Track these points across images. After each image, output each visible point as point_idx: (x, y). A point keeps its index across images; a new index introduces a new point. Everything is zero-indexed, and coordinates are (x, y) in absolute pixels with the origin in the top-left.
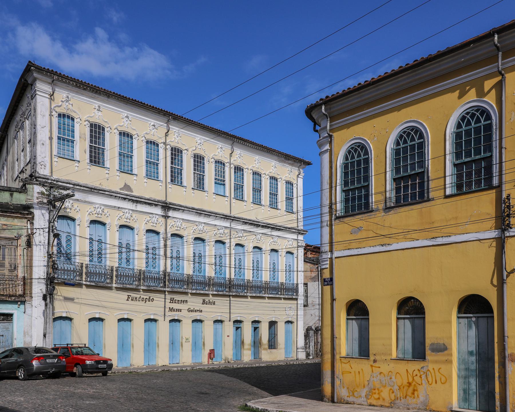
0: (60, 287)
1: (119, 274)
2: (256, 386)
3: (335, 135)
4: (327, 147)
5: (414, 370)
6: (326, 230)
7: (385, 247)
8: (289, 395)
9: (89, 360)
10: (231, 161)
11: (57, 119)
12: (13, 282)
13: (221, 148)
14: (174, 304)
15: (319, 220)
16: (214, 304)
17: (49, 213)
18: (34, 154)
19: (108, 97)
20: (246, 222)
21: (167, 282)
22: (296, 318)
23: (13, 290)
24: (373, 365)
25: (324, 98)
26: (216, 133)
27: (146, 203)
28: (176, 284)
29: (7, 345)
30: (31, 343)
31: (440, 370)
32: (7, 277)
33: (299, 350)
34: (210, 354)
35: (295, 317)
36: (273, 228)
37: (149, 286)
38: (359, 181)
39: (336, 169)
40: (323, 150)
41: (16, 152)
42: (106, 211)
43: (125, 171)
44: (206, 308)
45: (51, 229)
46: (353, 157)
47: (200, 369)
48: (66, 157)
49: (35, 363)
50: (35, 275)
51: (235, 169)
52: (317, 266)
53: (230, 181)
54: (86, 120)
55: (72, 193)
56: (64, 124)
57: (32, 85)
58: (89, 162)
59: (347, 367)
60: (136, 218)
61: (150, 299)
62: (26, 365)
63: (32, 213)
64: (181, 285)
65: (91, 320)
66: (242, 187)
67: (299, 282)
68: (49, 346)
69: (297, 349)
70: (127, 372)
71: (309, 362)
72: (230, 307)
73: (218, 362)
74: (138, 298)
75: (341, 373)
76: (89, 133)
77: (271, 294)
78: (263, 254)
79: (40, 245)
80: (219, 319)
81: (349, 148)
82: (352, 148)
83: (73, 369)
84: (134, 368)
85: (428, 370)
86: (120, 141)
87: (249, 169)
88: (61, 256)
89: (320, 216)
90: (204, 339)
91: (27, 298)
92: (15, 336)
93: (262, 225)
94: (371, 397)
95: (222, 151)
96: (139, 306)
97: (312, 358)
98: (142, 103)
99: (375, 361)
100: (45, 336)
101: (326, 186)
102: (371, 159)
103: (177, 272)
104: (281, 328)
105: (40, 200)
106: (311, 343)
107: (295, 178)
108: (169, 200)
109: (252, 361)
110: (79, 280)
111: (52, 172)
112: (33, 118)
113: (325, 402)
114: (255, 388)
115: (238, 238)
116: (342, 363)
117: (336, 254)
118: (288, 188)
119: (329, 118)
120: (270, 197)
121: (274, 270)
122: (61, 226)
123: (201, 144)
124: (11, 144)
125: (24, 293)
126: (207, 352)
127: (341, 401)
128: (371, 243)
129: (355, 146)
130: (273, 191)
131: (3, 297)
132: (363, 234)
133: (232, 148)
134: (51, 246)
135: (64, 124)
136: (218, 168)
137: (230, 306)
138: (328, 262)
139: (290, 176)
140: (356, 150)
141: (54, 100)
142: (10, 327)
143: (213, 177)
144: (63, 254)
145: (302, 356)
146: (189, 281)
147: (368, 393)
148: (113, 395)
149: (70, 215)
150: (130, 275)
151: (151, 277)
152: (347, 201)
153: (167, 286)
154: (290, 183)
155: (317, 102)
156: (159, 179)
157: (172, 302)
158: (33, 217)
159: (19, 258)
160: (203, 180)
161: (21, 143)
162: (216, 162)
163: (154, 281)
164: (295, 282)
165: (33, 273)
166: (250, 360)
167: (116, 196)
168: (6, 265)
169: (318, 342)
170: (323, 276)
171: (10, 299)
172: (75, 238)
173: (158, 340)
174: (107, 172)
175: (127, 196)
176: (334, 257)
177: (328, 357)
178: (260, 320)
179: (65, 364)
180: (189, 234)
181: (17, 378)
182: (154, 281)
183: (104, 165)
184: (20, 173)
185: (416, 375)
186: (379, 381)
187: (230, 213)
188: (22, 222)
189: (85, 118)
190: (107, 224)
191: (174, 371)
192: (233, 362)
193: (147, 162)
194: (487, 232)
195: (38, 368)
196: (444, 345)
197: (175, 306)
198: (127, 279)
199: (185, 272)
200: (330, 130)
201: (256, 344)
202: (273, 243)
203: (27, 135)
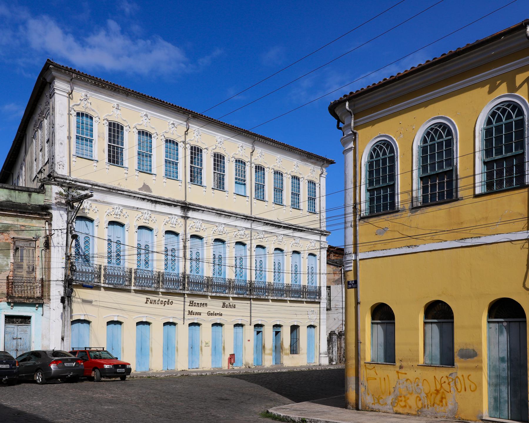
0: (78, 289)
1: (138, 276)
4: (352, 145)
5: (443, 377)
6: (350, 231)
8: (312, 402)
9: (107, 364)
10: (252, 160)
11: (75, 118)
12: (31, 284)
13: (242, 147)
14: (193, 307)
16: (234, 307)
17: (68, 214)
18: (52, 153)
19: (127, 95)
20: (268, 223)
21: (186, 285)
22: (319, 322)
24: (400, 371)
25: (348, 94)
27: (165, 204)
29: (25, 348)
31: (470, 377)
33: (321, 355)
34: (230, 358)
36: (295, 229)
37: (169, 289)
38: (384, 180)
39: (361, 168)
40: (347, 148)
41: (35, 152)
42: (124, 211)
44: (225, 311)
45: (69, 230)
48: (85, 157)
49: (52, 366)
50: (53, 278)
51: (256, 168)
54: (105, 119)
55: (91, 194)
56: (83, 123)
57: (50, 84)
58: (107, 162)
59: (371, 373)
60: (155, 219)
61: (169, 302)
62: (44, 369)
63: (50, 214)
64: (200, 287)
65: (109, 323)
66: (263, 187)
67: (322, 285)
68: (67, 348)
69: (320, 354)
70: (145, 377)
75: (365, 379)
76: (108, 132)
77: (293, 297)
79: (58, 247)
80: (240, 323)
81: (374, 146)
82: (377, 146)
83: (91, 373)
84: (154, 373)
85: (457, 377)
87: (271, 169)
88: (79, 258)
90: (224, 343)
92: (33, 339)
93: (284, 226)
94: (398, 404)
98: (161, 101)
99: (401, 367)
100: (63, 339)
101: (350, 185)
102: (397, 158)
104: (303, 332)
105: (58, 200)
106: (334, 348)
108: (189, 201)
110: (97, 282)
111: (70, 172)
113: (349, 409)
114: (277, 395)
121: (296, 272)
122: (79, 226)
123: (221, 143)
125: (42, 296)
126: (227, 356)
129: (380, 144)
130: (295, 191)
131: (21, 300)
132: (388, 236)
133: (253, 146)
134: (69, 247)
135: (83, 123)
136: (239, 167)
137: (251, 309)
138: (352, 264)
139: (312, 175)
140: (381, 148)
141: (72, 99)
144: (81, 255)
146: (209, 284)
147: (393, 400)
149: (89, 216)
150: (149, 277)
152: (371, 200)
153: (186, 289)
156: (178, 179)
157: (191, 305)
158: (52, 218)
161: (40, 143)
162: (236, 161)
164: (318, 285)
166: (272, 366)
167: (134, 197)
168: (24, 267)
169: (341, 347)
171: (28, 302)
173: (177, 344)
175: (146, 196)
176: (358, 259)
177: (352, 362)
178: (281, 324)
180: (209, 235)
181: (35, 382)
182: (173, 283)
183: (123, 165)
184: (38, 173)
185: (445, 382)
187: (251, 214)
188: (40, 223)
189: (103, 117)
190: (125, 225)
191: (193, 376)
192: (253, 367)
193: (166, 161)
194: (519, 233)
195: (55, 372)
196: (474, 350)
197: (195, 309)
198: (146, 281)
201: (278, 348)
202: (295, 245)
203: (46, 135)
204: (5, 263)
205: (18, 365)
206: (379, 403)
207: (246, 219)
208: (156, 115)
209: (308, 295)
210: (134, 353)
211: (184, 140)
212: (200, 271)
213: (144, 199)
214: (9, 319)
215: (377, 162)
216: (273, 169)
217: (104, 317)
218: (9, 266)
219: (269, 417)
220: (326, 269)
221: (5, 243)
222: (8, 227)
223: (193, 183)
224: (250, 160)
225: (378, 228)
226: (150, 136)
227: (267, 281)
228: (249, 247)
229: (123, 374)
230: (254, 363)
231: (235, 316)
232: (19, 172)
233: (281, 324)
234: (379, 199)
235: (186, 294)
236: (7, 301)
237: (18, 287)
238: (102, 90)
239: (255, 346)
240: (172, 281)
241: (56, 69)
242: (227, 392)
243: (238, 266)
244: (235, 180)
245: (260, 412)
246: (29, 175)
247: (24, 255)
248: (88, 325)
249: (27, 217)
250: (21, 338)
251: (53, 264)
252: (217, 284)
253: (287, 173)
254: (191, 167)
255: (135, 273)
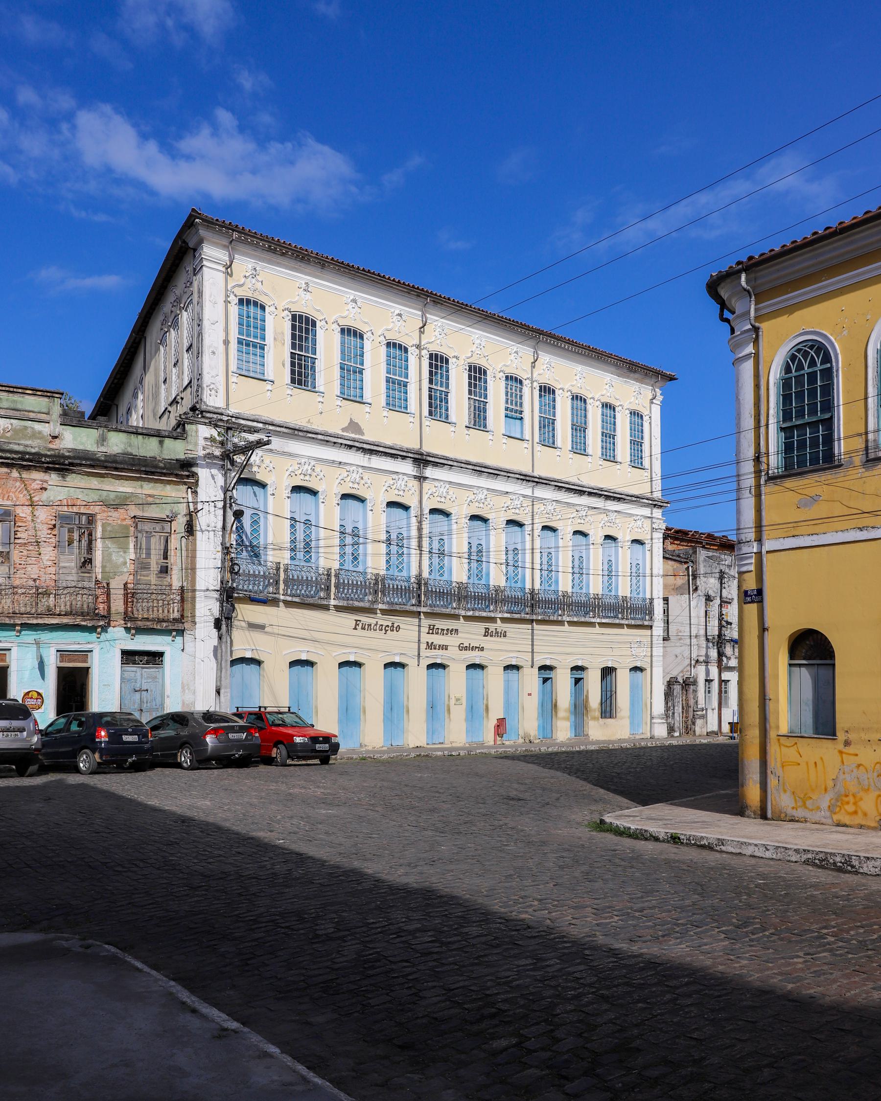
0: (240, 605)
1: (342, 581)
2: (602, 787)
3: (764, 326)
4: (750, 349)
6: (748, 504)
7: (866, 531)
8: (671, 804)
9: (299, 736)
10: (534, 376)
11: (237, 307)
12: (164, 596)
13: (516, 352)
14: (435, 636)
15: (734, 486)
16: (505, 636)
17: (225, 475)
18: (198, 370)
19: (323, 266)
20: (561, 486)
21: (423, 596)
22: (649, 661)
23: (163, 611)
24: (844, 750)
25: (745, 260)
26: (508, 325)
27: (386, 454)
28: (439, 600)
29: (154, 707)
30: (193, 703)
32: (154, 587)
33: (654, 721)
34: (498, 726)
35: (649, 660)
36: (608, 498)
37: (392, 603)
38: (813, 411)
39: (768, 389)
40: (741, 355)
41: (163, 368)
42: (318, 469)
43: (349, 398)
44: (489, 643)
45: (228, 502)
46: (800, 367)
47: (483, 753)
48: (252, 374)
49: (209, 739)
50: (200, 585)
51: (540, 390)
52: (686, 566)
53: (532, 411)
54: (285, 309)
56: (248, 317)
57: (195, 250)
59: (791, 753)
60: (369, 482)
61: (393, 626)
62: (194, 743)
63: (194, 475)
64: (447, 601)
65: (293, 664)
66: (553, 423)
67: (654, 596)
68: (226, 707)
69: (652, 718)
70: (356, 759)
71: (674, 742)
72: (532, 641)
73: (512, 742)
74: (373, 625)
75: (779, 765)
76: (290, 331)
77: (604, 617)
78: (620, 549)
79: (209, 531)
80: (514, 663)
81: (793, 351)
82: (799, 351)
83: (271, 751)
84: (367, 751)
86: (343, 344)
87: (565, 390)
88: (242, 550)
89: (735, 479)
90: (487, 700)
91: (186, 625)
92: (168, 692)
94: (841, 809)
95: (518, 358)
96: (375, 639)
97: (678, 734)
98: (380, 276)
99: (847, 743)
100: (218, 692)
101: (748, 422)
102: (837, 371)
103: (439, 578)
104: (623, 679)
105: (208, 451)
106: (676, 708)
107: (647, 404)
108: (426, 449)
109: (571, 739)
110: (273, 593)
111: (228, 405)
112: (197, 308)
113: (748, 817)
114: (602, 791)
115: (513, 511)
116: (782, 747)
117: (768, 546)
118: (635, 424)
119: (753, 298)
120: (602, 441)
121: (610, 573)
122: (243, 495)
123: (481, 347)
124: (153, 354)
125: (182, 616)
126: (493, 722)
127: (780, 816)
128: (839, 526)
129: (805, 346)
130: (607, 429)
131: (148, 623)
132: (820, 510)
133: (535, 352)
134: (229, 532)
135: (248, 317)
136: (511, 389)
137: (532, 639)
138: (753, 561)
139: (637, 402)
140: (806, 354)
141: (231, 275)
142: (159, 676)
143: (503, 406)
144: (246, 546)
145: (661, 731)
146: (462, 594)
147: (833, 802)
148: (359, 800)
149: (259, 477)
150: (359, 583)
151: (395, 587)
152: (788, 448)
153: (422, 604)
154: (638, 414)
155: (731, 267)
156: (408, 411)
157: (431, 631)
158: (197, 481)
159: (172, 554)
160: (485, 412)
161: (173, 352)
162: (507, 377)
163: (401, 594)
164: (648, 596)
165: (198, 579)
166: (569, 739)
167: (335, 443)
169: (688, 706)
170: (742, 586)
171: (159, 627)
172: (267, 518)
173: (408, 701)
174: (321, 399)
176: (764, 551)
177: (753, 734)
178: (585, 664)
179: (259, 741)
180: (461, 511)
181: (179, 766)
182: (401, 594)
183: (315, 388)
184: (171, 405)
186: (856, 780)
187: (533, 471)
188: (178, 490)
189: (282, 305)
190: (320, 493)
191: (437, 756)
192: (538, 741)
193: (388, 380)
195: (214, 749)
197: (437, 639)
198: (355, 591)
199: (454, 579)
200: (756, 318)
201: (580, 708)
202: (609, 524)
203: (185, 337)
204: (122, 560)
205: (151, 737)
206: (804, 805)
207: (523, 480)
208: (376, 302)
209: (631, 614)
210: (335, 716)
211: (418, 343)
212: (446, 572)
213: (351, 447)
214: (129, 656)
215: (799, 379)
216: (570, 391)
217: (284, 653)
218: (128, 565)
219: (608, 831)
220: (661, 567)
221: (121, 525)
222: (126, 498)
223: (433, 417)
224: (530, 376)
225: (801, 497)
226: (361, 337)
227: (560, 589)
228: (530, 528)
229: (325, 754)
230: (539, 735)
231: (506, 651)
232: (130, 403)
233: (584, 664)
234: (802, 444)
235: (422, 614)
236: (125, 626)
237: (142, 602)
238: (281, 259)
239: (540, 704)
240: (398, 590)
241: (204, 225)
242: (516, 786)
243: (511, 563)
244: (505, 412)
245: (586, 823)
246: (151, 407)
247: (153, 547)
248: (258, 667)
249: (156, 481)
250: (147, 690)
251: (200, 562)
252: (475, 595)
253: (593, 398)
254: (430, 389)
255: (337, 576)
